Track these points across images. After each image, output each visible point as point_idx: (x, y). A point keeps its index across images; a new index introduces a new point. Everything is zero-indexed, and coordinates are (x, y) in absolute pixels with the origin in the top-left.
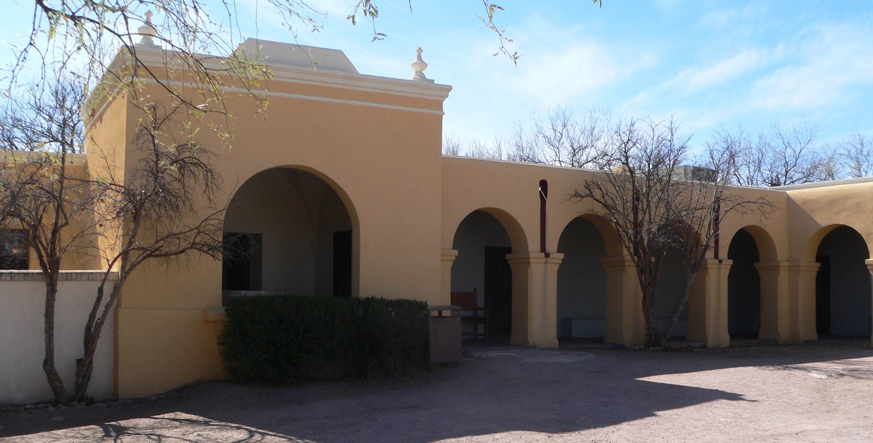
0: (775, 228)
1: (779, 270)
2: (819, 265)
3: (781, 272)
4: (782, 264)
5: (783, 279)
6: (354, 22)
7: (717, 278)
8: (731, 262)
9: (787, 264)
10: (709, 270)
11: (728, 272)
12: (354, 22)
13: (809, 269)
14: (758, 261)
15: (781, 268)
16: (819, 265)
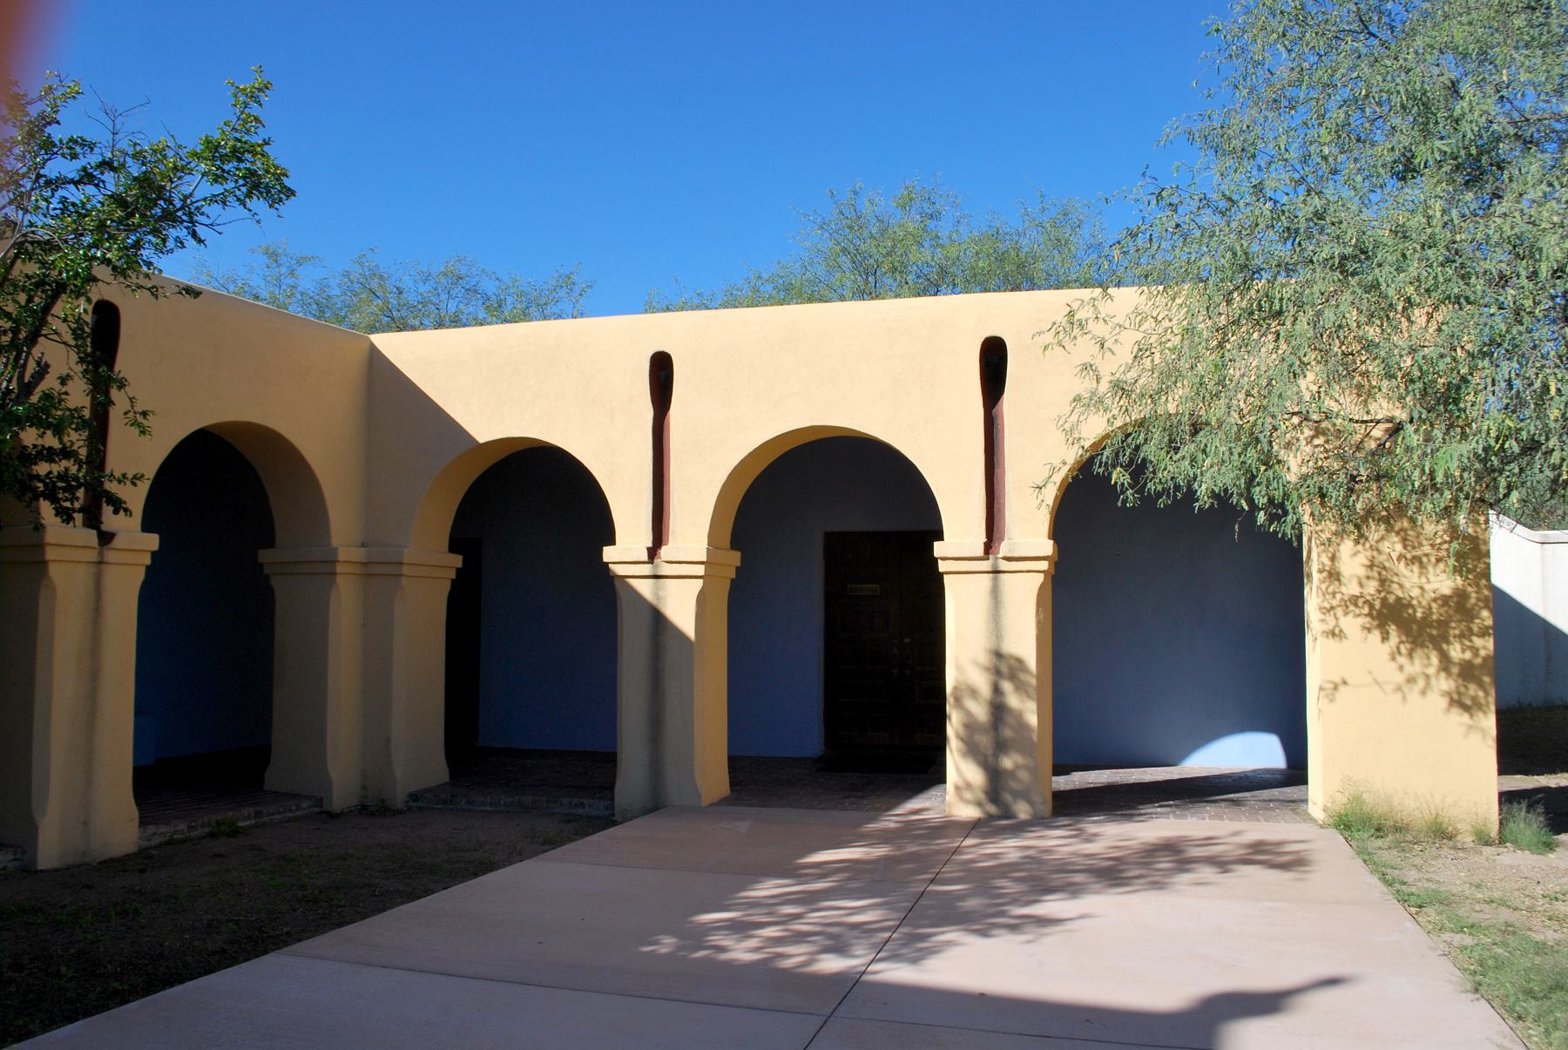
0: (319, 430)
1: (44, 564)
2: (457, 560)
3: (339, 579)
4: (341, 556)
5: (345, 603)
6: (265, 88)
7: (96, 590)
8: (153, 541)
9: (358, 554)
10: (53, 569)
11: (139, 576)
12: (265, 88)
13: (430, 566)
14: (612, 542)
15: (339, 569)
16: (457, 560)
